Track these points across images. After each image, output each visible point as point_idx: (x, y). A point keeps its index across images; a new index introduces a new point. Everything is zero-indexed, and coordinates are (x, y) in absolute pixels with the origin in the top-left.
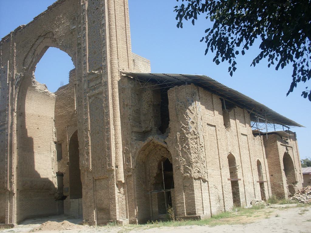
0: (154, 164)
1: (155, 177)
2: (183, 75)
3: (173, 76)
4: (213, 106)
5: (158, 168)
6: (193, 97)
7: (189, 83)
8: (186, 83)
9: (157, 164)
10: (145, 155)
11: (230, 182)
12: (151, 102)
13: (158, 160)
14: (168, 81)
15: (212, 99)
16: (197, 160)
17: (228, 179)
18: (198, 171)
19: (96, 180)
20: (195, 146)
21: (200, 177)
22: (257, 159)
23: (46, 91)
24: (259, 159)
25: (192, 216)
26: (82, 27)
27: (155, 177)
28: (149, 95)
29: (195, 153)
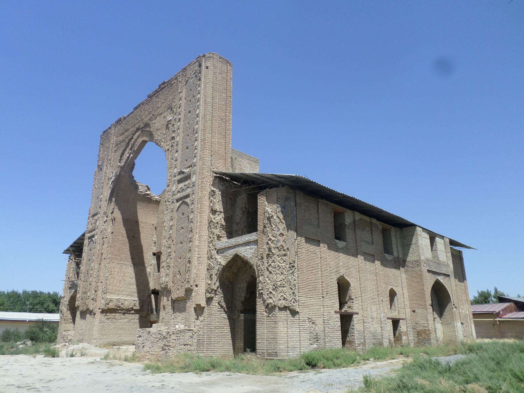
0: (242, 286)
1: (243, 302)
2: (276, 176)
3: (268, 176)
4: (318, 216)
5: (247, 290)
6: (286, 203)
7: (283, 185)
8: (280, 185)
9: (245, 285)
10: (233, 273)
11: (338, 316)
12: (246, 208)
13: (247, 280)
14: (263, 182)
15: (318, 206)
16: (284, 283)
17: (336, 312)
18: (284, 298)
19: (174, 301)
20: (282, 265)
21: (287, 305)
22: (391, 287)
23: (148, 192)
24: (393, 288)
25: (58, 357)
26: (177, 118)
27: (243, 302)
28: (243, 200)
29: (282, 273)
